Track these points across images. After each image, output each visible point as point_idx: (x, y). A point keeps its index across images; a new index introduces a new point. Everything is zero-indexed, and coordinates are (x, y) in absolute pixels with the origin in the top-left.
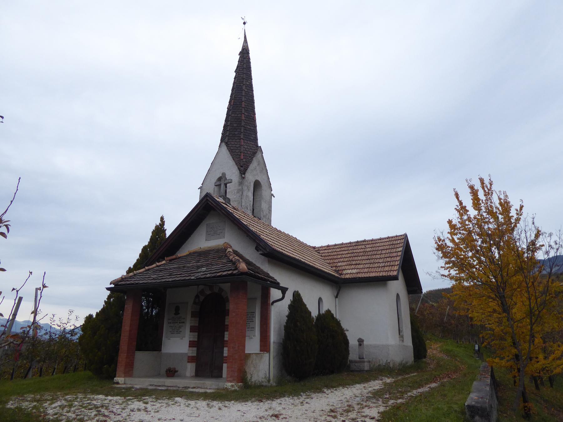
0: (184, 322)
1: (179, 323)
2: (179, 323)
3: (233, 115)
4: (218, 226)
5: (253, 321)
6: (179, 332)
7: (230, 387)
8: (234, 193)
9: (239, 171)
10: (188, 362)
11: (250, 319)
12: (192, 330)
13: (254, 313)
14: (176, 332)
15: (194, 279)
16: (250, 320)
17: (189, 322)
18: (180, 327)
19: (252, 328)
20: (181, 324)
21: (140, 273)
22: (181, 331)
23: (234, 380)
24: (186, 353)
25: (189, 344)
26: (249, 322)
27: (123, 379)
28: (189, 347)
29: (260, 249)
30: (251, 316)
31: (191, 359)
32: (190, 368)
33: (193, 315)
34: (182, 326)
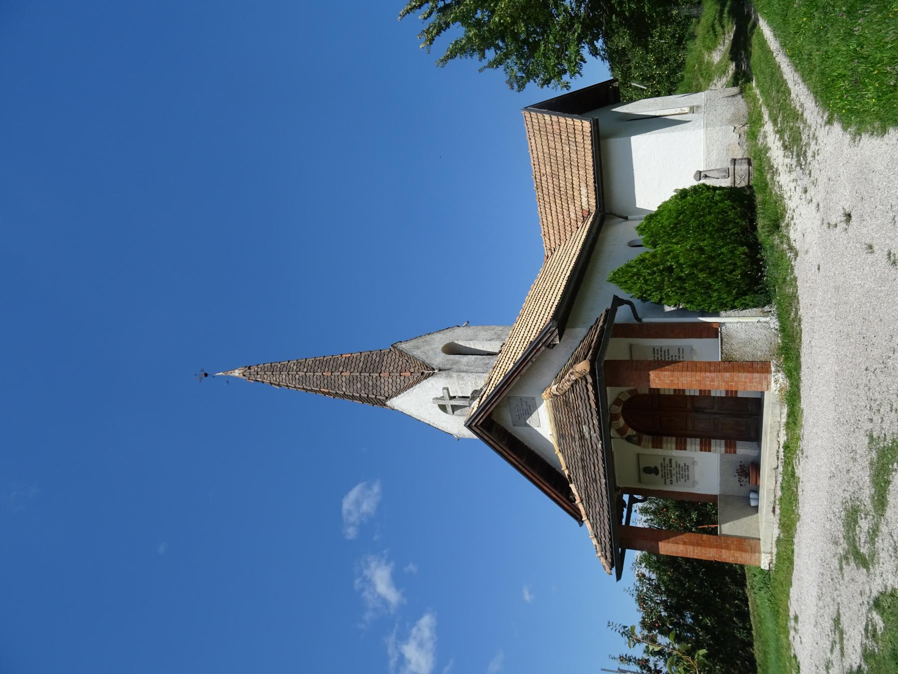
0: (670, 460)
1: (671, 467)
3: (344, 389)
4: (517, 408)
5: (668, 350)
6: (686, 467)
7: (778, 385)
8: (463, 386)
9: (430, 378)
10: (735, 452)
11: (665, 356)
12: (682, 446)
13: (654, 349)
16: (667, 354)
17: (670, 451)
18: (678, 465)
19: (679, 351)
20: (674, 465)
21: (593, 527)
22: (685, 464)
24: (721, 456)
25: (705, 451)
26: (670, 356)
27: (763, 556)
28: (710, 451)
29: (552, 341)
30: (660, 353)
31: (730, 446)
32: (743, 450)
33: (658, 444)
34: (676, 462)
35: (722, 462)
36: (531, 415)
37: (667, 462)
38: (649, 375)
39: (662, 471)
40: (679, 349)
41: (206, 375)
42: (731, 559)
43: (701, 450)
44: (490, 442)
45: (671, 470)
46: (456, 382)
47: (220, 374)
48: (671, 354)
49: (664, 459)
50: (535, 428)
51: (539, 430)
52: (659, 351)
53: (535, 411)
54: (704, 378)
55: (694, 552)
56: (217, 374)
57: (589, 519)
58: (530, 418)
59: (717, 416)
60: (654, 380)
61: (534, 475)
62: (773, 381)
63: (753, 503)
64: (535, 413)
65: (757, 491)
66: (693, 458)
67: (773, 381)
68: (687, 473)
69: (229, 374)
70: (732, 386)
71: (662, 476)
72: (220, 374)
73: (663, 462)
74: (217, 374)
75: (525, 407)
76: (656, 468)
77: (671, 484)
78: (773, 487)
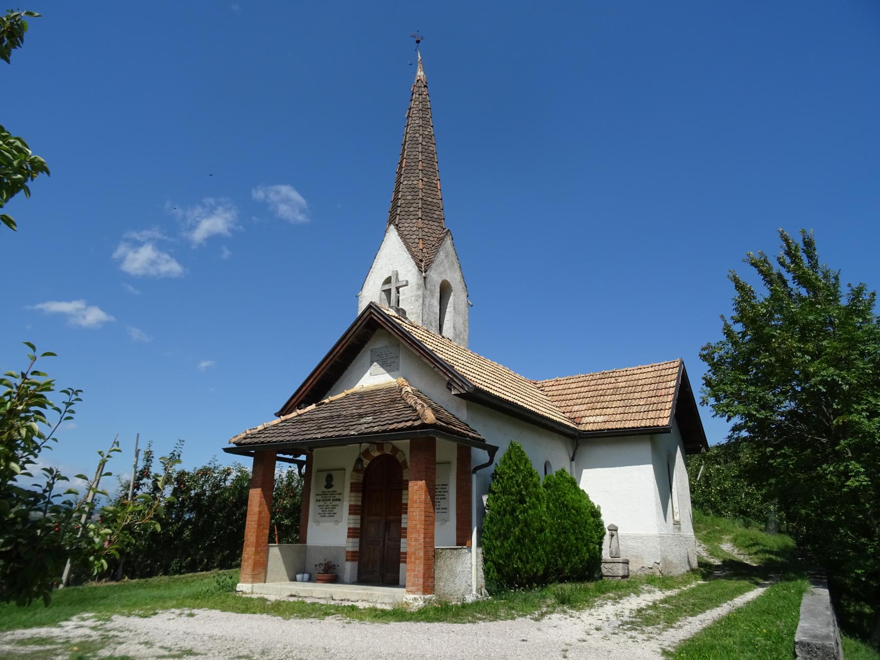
0: (339, 500)
1: (333, 500)
2: (333, 500)
3: (405, 182)
6: (332, 515)
10: (347, 560)
11: (440, 495)
12: (353, 510)
13: (446, 485)
14: (328, 514)
15: (354, 435)
17: (348, 500)
18: (334, 507)
19: (444, 509)
21: (274, 426)
22: (336, 513)
23: (418, 590)
25: (348, 533)
26: (439, 500)
27: (250, 585)
28: (348, 537)
30: (442, 490)
31: (353, 556)
32: (349, 568)
33: (354, 488)
34: (337, 505)
35: (337, 549)
36: (382, 367)
37: (338, 497)
38: (421, 480)
39: (329, 492)
40: (446, 509)
41: (418, 42)
42: (246, 556)
43: (349, 529)
44: (356, 327)
45: (329, 500)
46: (413, 294)
47: (419, 56)
48: (441, 501)
49: (340, 494)
50: (369, 371)
51: (367, 374)
52: (444, 490)
53: (386, 370)
54: (418, 532)
55: (252, 521)
56: (419, 53)
57: (282, 422)
58: (379, 366)
59: (381, 544)
60: (417, 485)
61: (323, 369)
62: (415, 596)
63: (299, 576)
64: (384, 371)
65: (310, 580)
66: (342, 521)
67: (415, 596)
68: (327, 515)
69: (420, 65)
70: (411, 558)
71: (323, 492)
72: (419, 56)
73: (338, 492)
74: (419, 53)
75: (389, 361)
76: (332, 486)
77: (317, 501)
78: (314, 595)
